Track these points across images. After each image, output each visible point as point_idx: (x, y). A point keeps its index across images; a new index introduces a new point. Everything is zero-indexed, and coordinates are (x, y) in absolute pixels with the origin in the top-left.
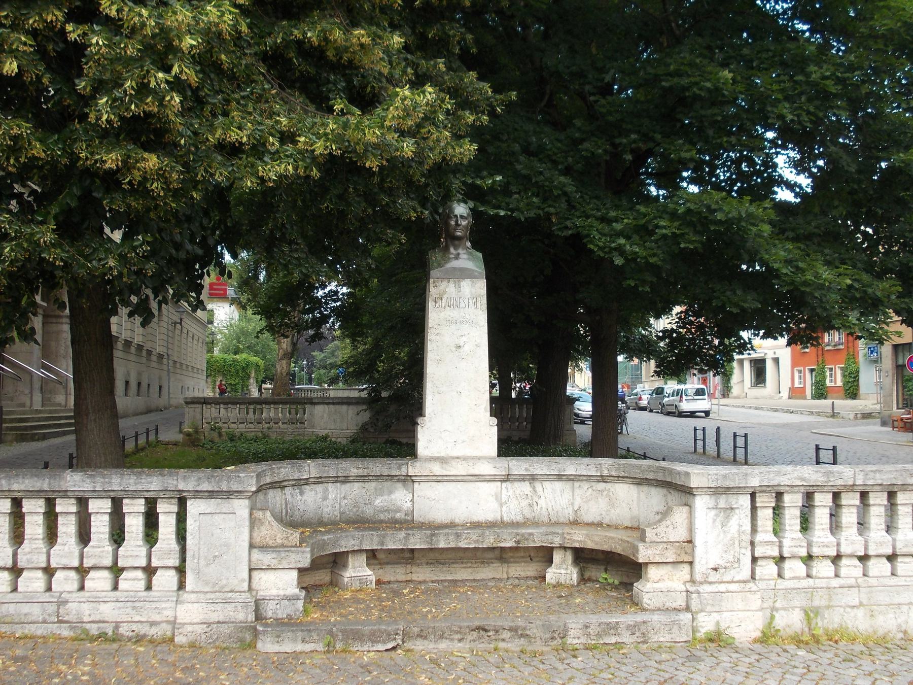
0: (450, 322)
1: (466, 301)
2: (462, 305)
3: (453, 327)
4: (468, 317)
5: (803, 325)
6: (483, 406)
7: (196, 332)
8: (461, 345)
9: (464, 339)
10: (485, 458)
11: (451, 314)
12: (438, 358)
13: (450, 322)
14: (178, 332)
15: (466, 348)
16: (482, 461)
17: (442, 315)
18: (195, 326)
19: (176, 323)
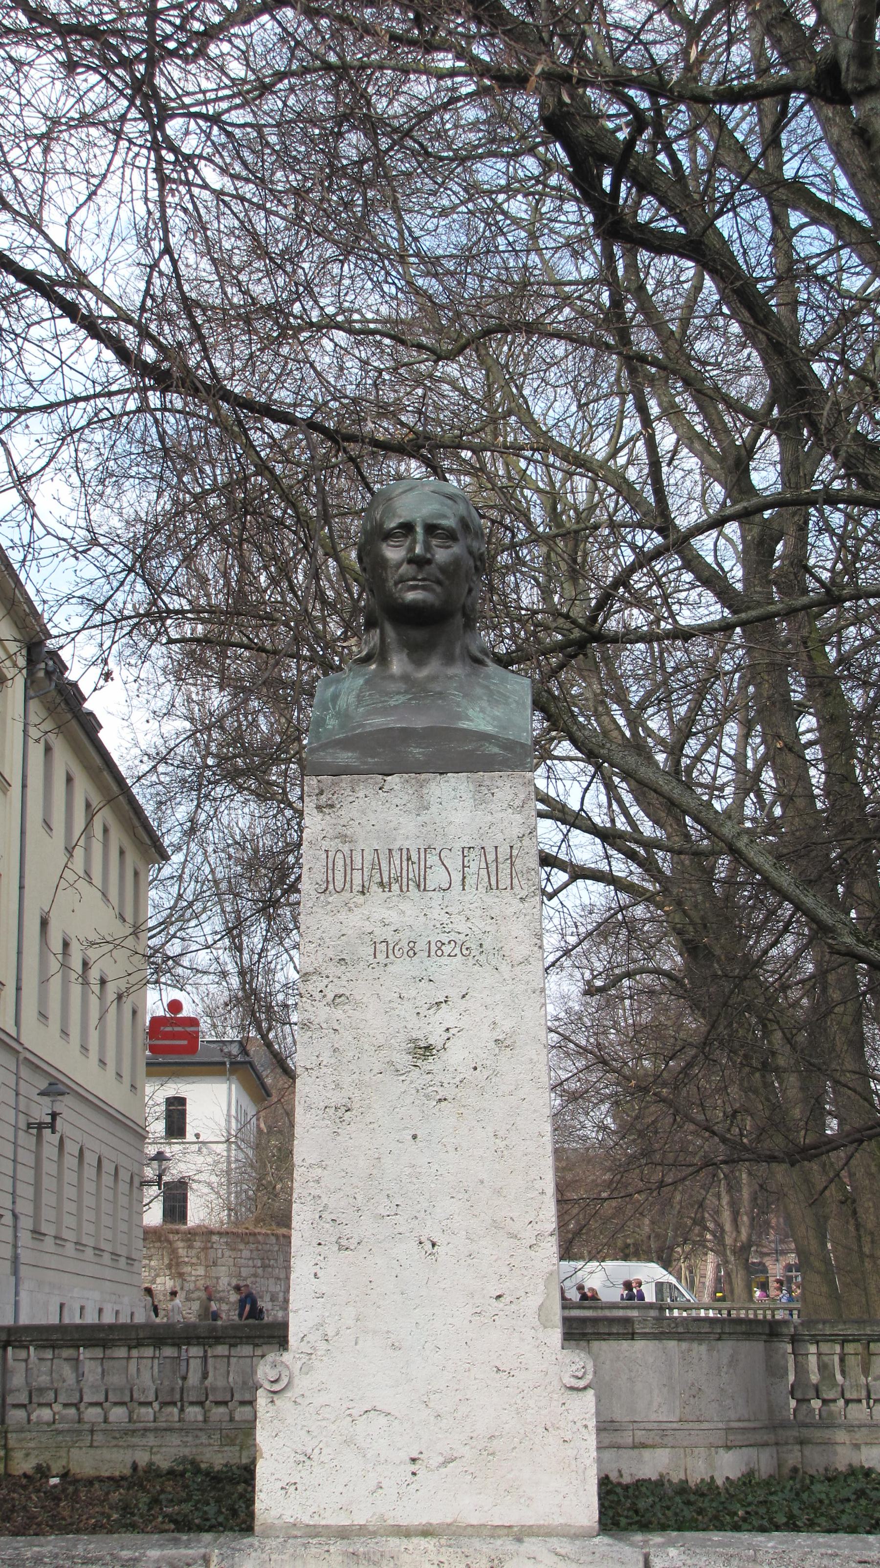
0: (387, 949)
1: (454, 862)
2: (437, 877)
3: (402, 967)
4: (463, 927)
5: (751, 689)
6: (533, 1302)
7: (106, 1152)
8: (436, 1040)
9: (448, 1016)
10: (544, 1532)
11: (392, 916)
12: (338, 1098)
13: (387, 949)
14: (50, 1151)
15: (456, 1056)
16: (531, 1545)
17: (354, 921)
18: (81, 1122)
19: (40, 1126)
